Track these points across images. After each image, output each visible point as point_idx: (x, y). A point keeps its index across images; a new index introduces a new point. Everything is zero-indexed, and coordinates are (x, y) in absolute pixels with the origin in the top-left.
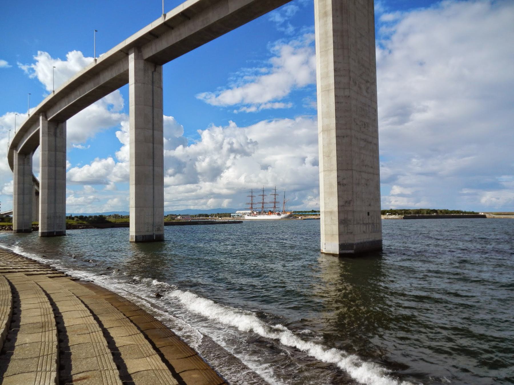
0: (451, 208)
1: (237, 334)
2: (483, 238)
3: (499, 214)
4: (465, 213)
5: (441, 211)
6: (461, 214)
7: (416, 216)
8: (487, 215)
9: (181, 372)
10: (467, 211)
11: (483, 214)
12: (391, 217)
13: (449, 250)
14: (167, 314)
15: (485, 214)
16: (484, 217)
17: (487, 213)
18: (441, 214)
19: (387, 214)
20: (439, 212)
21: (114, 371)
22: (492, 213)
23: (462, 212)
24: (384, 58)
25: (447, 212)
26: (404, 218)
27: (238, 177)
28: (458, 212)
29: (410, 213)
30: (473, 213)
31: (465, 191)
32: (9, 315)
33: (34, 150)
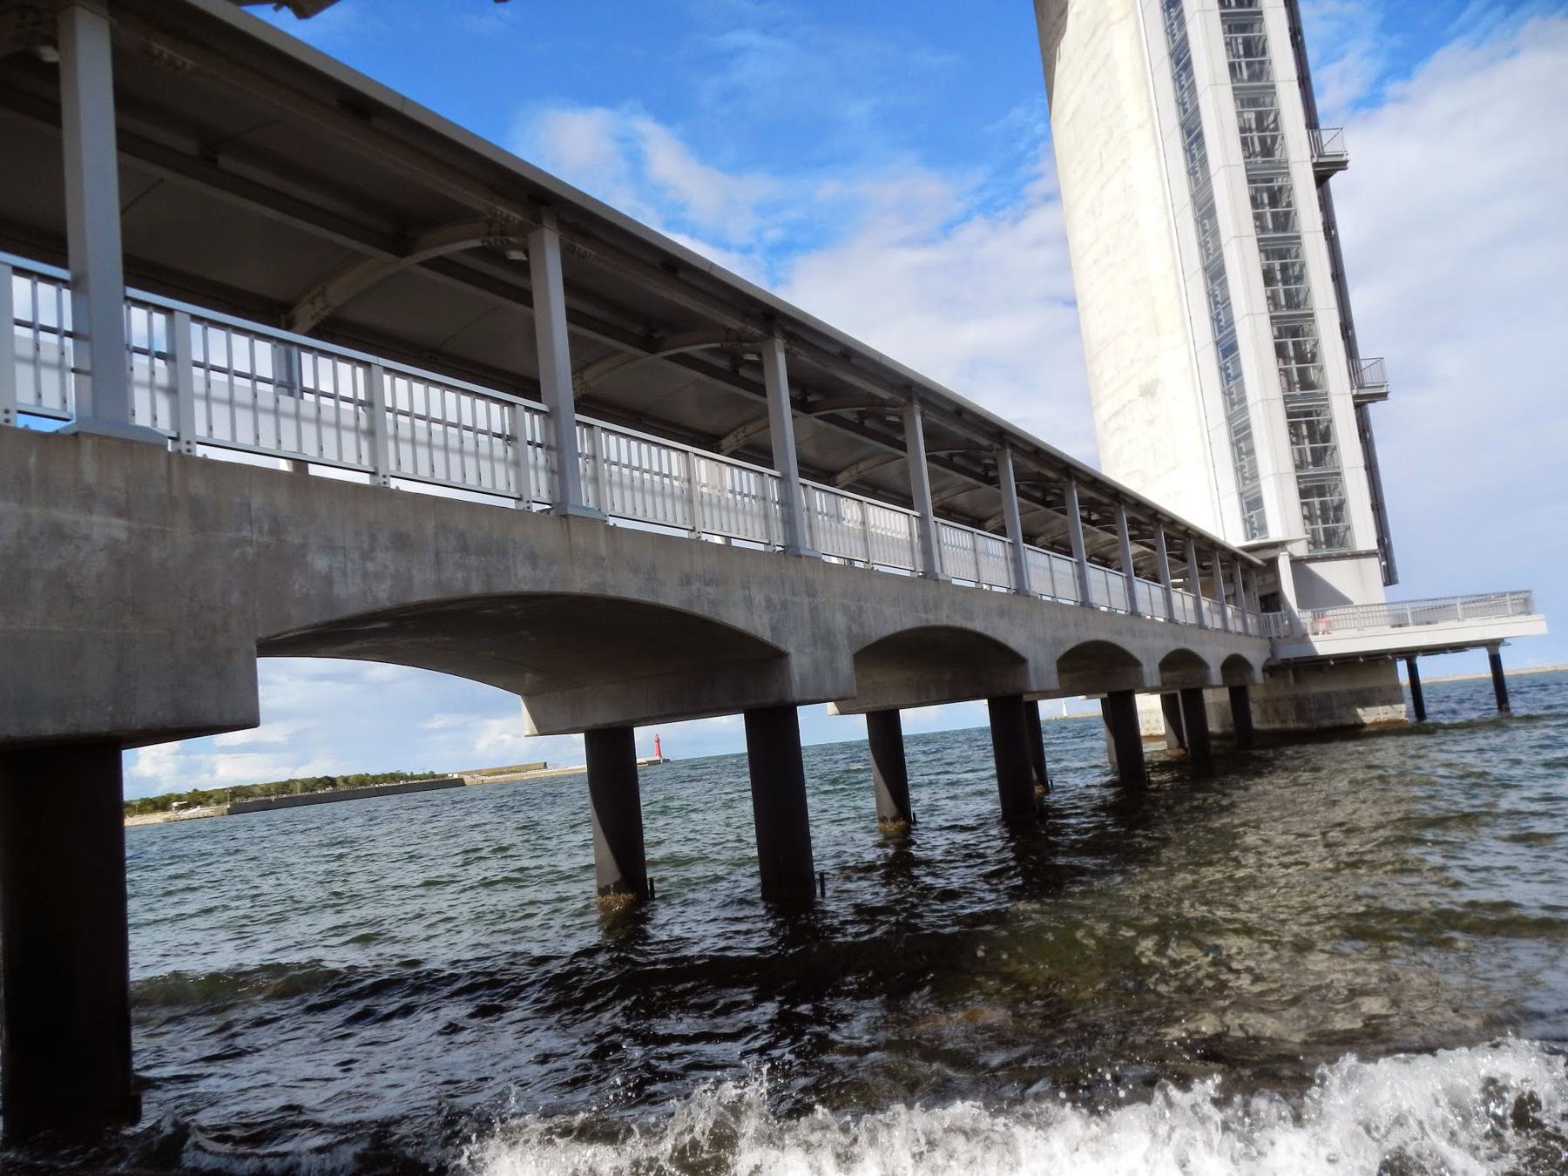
0: (377, 767)
2: (476, 826)
3: (495, 774)
4: (413, 777)
5: (346, 780)
7: (270, 801)
8: (467, 779)
9: (1471, 727)
10: (417, 772)
11: (456, 776)
12: (185, 814)
13: (1319, 774)
16: (460, 783)
17: (465, 773)
18: (343, 788)
19: (175, 804)
20: (340, 782)
21: (996, 1128)
22: (479, 772)
23: (406, 778)
25: (362, 780)
26: (230, 812)
27: (1152, 738)
28: (393, 777)
31: (438, 722)
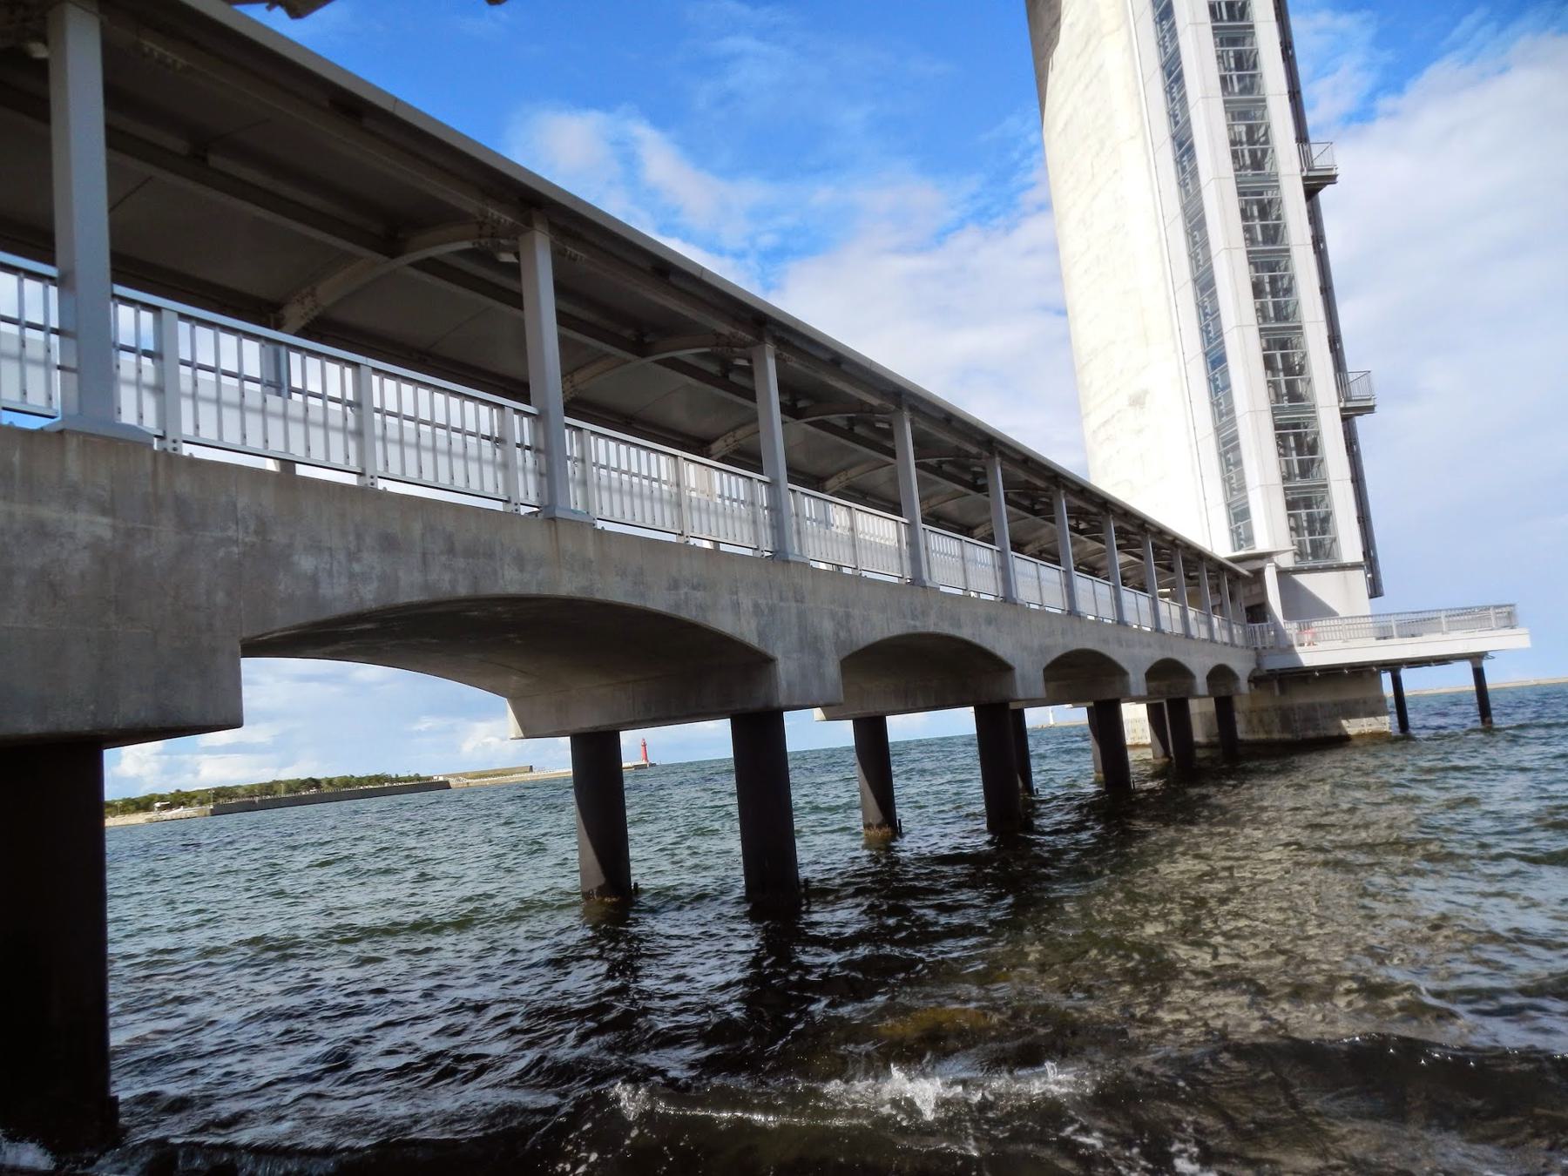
1: (753, 954)
4: (398, 779)
5: (330, 782)
6: (386, 785)
8: (452, 782)
11: (441, 779)
14: (259, 1061)
15: (447, 779)
16: (445, 785)
17: (453, 776)
22: (465, 775)
24: (1301, 1032)
25: (347, 782)
26: (214, 813)
28: (378, 779)
29: (237, 796)
30: (418, 778)
31: (426, 723)
32: (520, 1103)
33: (929, 465)
